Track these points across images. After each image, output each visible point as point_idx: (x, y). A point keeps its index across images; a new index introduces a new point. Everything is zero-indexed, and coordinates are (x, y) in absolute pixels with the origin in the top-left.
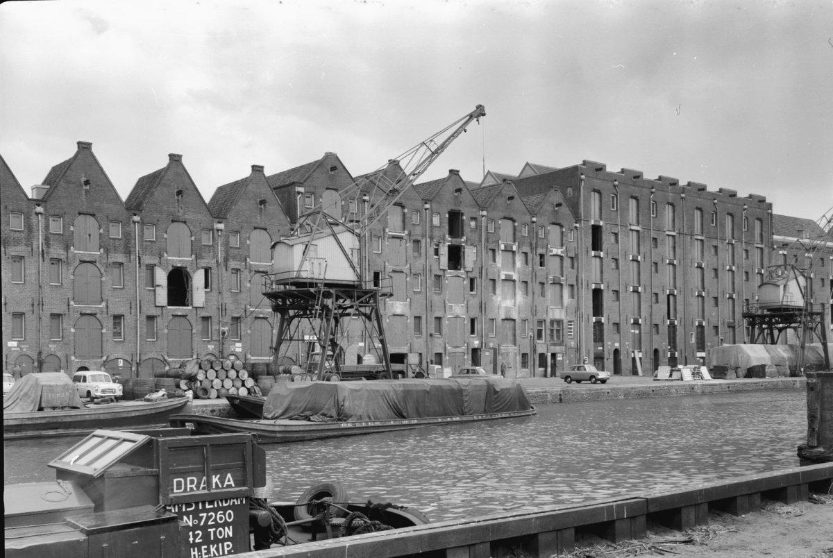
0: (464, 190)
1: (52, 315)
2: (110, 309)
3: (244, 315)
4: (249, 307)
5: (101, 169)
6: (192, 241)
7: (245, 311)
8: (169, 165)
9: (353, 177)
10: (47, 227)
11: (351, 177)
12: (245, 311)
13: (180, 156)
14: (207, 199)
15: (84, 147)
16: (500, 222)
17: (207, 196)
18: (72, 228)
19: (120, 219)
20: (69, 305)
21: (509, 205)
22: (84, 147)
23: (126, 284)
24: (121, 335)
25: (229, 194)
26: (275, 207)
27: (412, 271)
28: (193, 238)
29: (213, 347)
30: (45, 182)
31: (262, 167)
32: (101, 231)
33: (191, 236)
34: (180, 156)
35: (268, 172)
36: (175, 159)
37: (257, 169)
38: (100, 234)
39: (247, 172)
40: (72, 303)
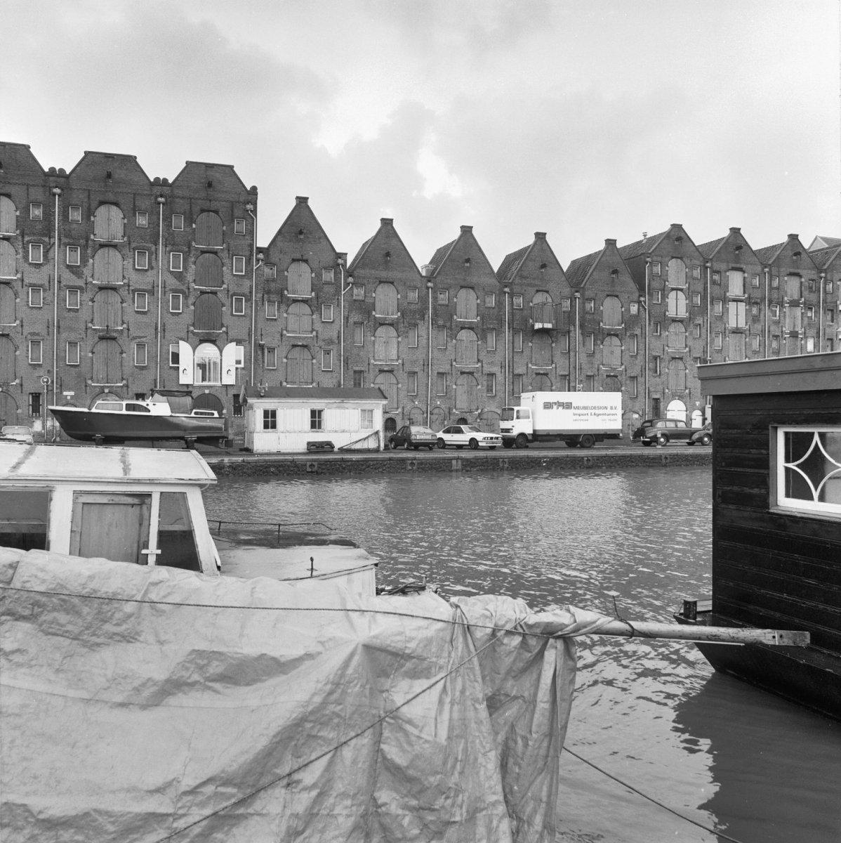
0: (804, 255)
1: (438, 373)
2: (484, 369)
3: (596, 373)
4: (601, 366)
5: (480, 249)
6: (398, 299)
7: (598, 370)
8: (535, 243)
9: (696, 245)
10: (512, 304)
11: (694, 244)
12: (598, 370)
13: (545, 234)
14: (565, 270)
15: (540, 237)
16: (786, 278)
17: (496, 265)
18: (455, 300)
19: (494, 291)
20: (452, 365)
21: (738, 254)
22: (540, 237)
23: (498, 346)
24: (492, 391)
25: (582, 267)
26: (626, 279)
27: (752, 332)
28: (623, 309)
29: (73, 393)
30: (431, 263)
31: (392, 220)
32: (479, 301)
33: (477, 299)
34: (545, 234)
35: (619, 245)
36: (467, 231)
37: (611, 243)
38: (478, 304)
39: (601, 246)
40: (454, 363)
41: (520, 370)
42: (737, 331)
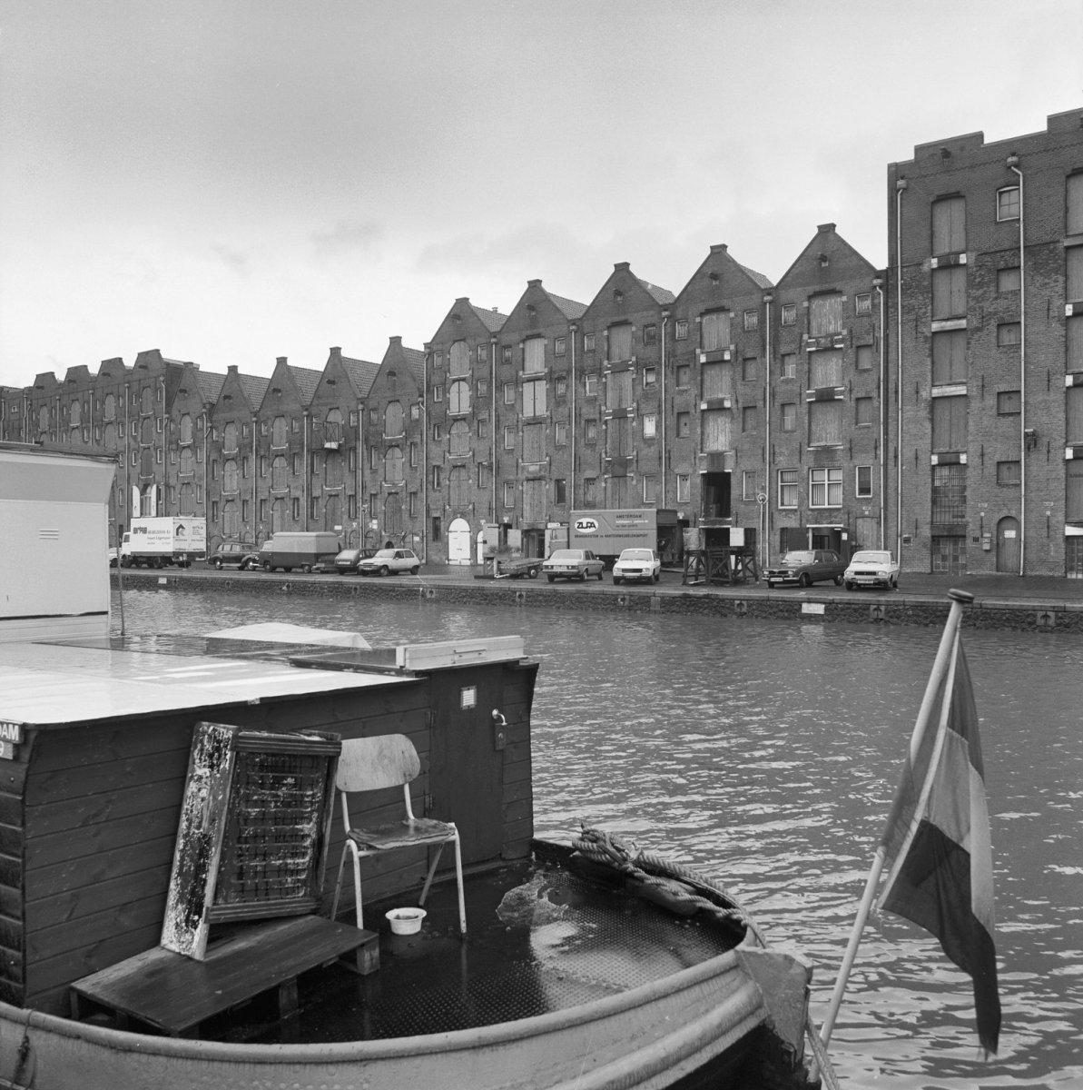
41: (316, 493)
42: (535, 421)
